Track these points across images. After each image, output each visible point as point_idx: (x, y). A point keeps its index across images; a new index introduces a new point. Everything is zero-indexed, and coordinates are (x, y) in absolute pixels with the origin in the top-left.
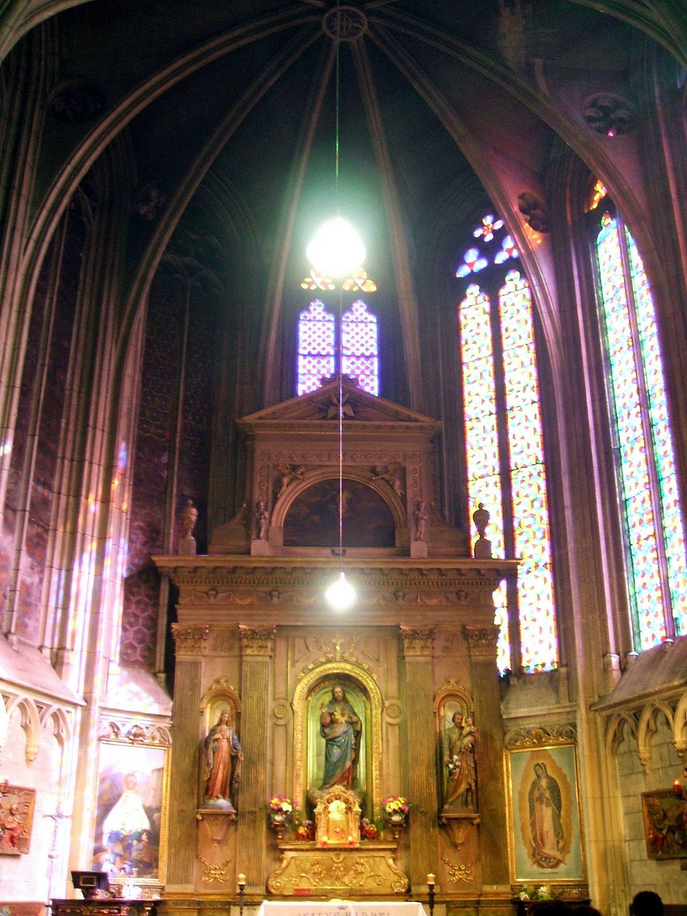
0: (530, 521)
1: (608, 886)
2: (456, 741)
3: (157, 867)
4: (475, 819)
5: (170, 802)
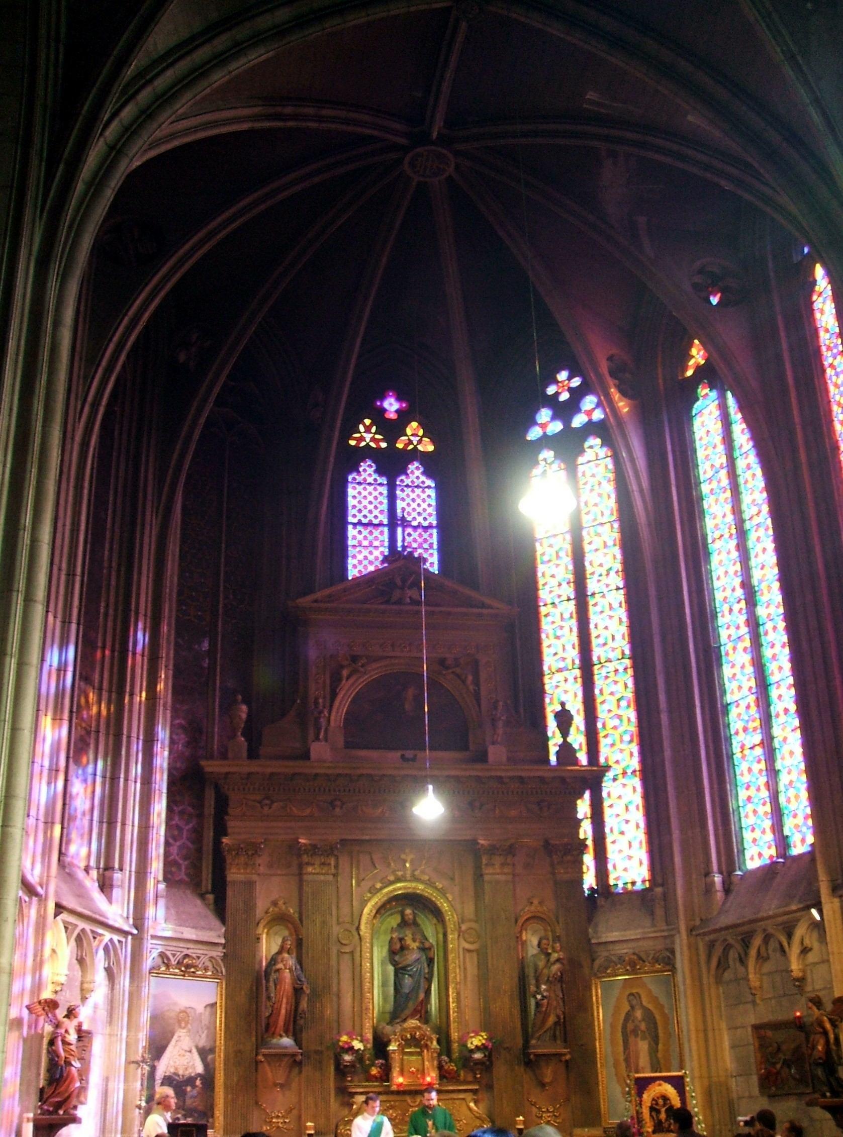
0: (616, 722)
1: (714, 1126)
2: (543, 969)
3: (212, 1116)
4: (565, 1055)
5: (225, 1042)
